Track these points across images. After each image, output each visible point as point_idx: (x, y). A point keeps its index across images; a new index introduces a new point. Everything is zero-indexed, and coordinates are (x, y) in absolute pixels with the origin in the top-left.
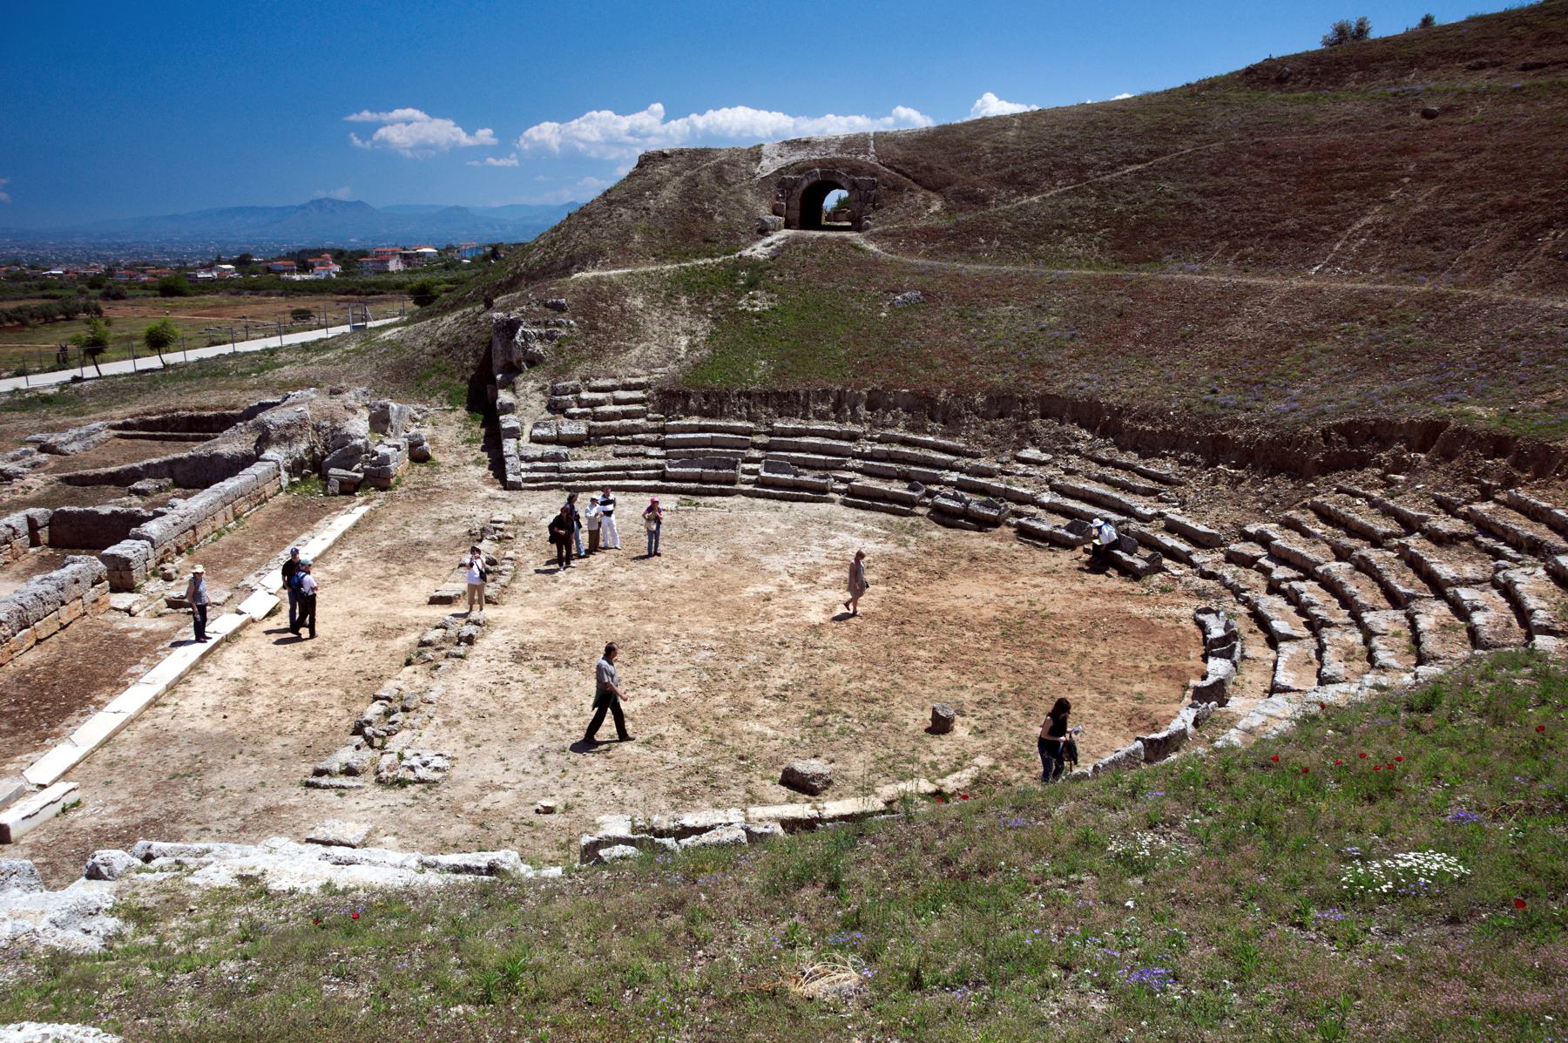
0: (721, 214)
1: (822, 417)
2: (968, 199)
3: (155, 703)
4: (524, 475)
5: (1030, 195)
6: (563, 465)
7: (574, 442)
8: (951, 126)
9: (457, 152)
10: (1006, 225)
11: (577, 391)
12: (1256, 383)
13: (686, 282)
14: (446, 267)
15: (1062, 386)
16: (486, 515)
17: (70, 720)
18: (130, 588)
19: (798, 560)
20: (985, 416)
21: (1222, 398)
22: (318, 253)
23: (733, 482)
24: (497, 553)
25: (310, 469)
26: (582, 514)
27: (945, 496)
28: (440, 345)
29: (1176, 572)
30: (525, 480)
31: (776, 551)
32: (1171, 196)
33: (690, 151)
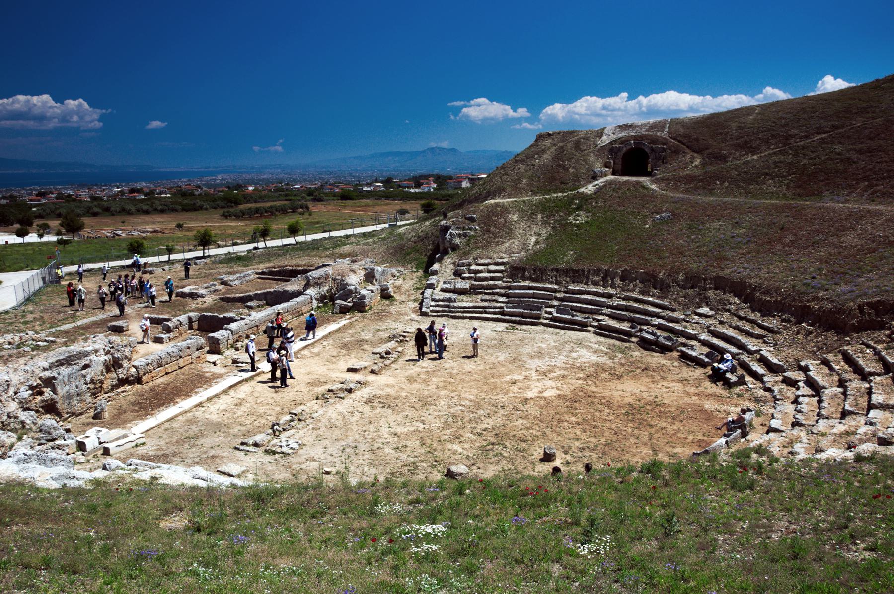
1: (596, 284)
2: (716, 158)
3: (200, 405)
5: (753, 155)
6: (452, 304)
9: (507, 121)
11: (470, 265)
13: (543, 207)
17: (161, 409)
18: (218, 352)
20: (684, 287)
22: (426, 177)
23: (539, 318)
25: (327, 300)
27: (648, 333)
30: (431, 311)
32: (839, 154)
33: (564, 132)
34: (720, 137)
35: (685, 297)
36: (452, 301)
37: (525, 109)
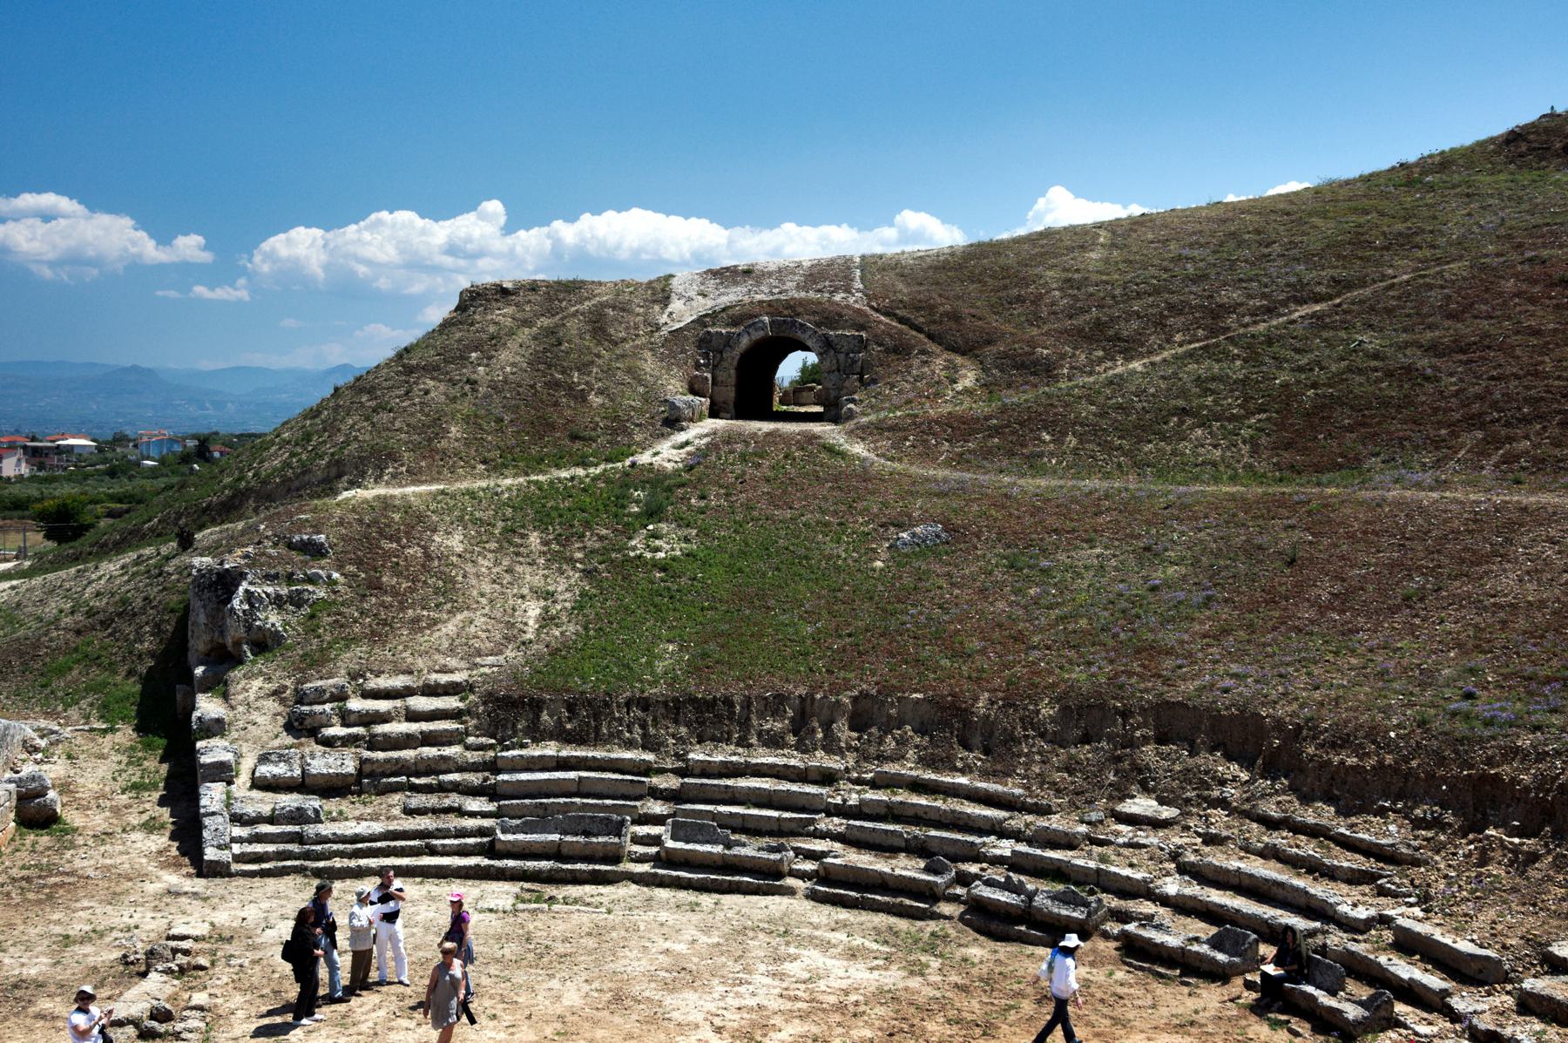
0: (600, 392)
2: (1021, 366)
4: (236, 849)
5: (1128, 359)
6: (311, 830)
7: (332, 788)
8: (991, 244)
9: (137, 270)
10: (1087, 410)
11: (341, 697)
12: (1548, 680)
13: (539, 510)
14: (112, 473)
15: (1191, 687)
16: (160, 924)
19: (731, 1001)
20: (1059, 741)
21: (1482, 708)
23: (616, 860)
24: (173, 998)
26: (341, 920)
27: (990, 883)
28: (91, 613)
29: (1423, 1029)
30: (238, 859)
31: (691, 985)
32: (1376, 356)
33: (548, 285)
34: (1018, 310)
35: (1070, 771)
36: (308, 821)
37: (200, 239)
